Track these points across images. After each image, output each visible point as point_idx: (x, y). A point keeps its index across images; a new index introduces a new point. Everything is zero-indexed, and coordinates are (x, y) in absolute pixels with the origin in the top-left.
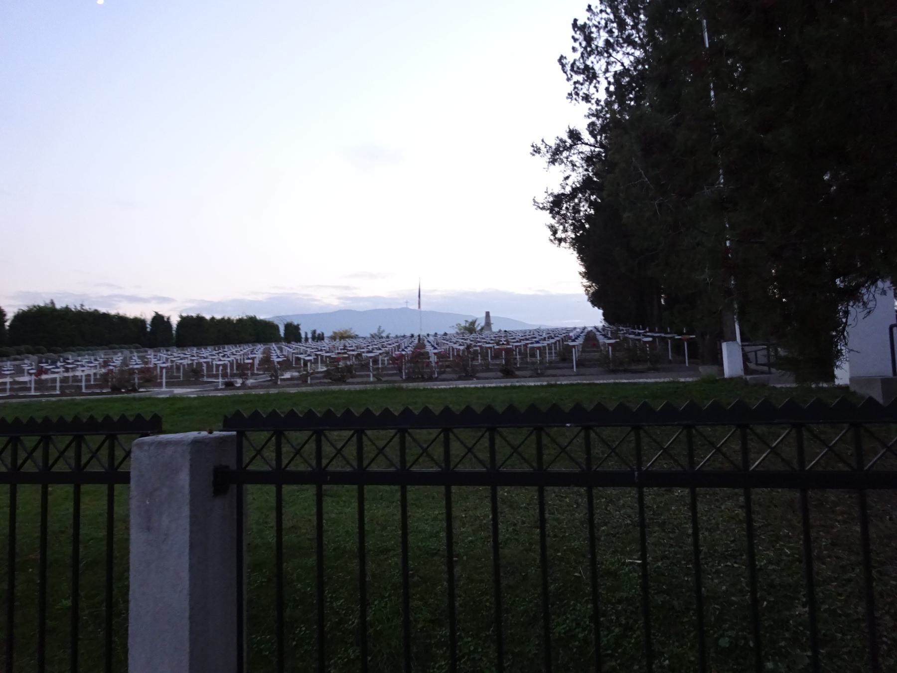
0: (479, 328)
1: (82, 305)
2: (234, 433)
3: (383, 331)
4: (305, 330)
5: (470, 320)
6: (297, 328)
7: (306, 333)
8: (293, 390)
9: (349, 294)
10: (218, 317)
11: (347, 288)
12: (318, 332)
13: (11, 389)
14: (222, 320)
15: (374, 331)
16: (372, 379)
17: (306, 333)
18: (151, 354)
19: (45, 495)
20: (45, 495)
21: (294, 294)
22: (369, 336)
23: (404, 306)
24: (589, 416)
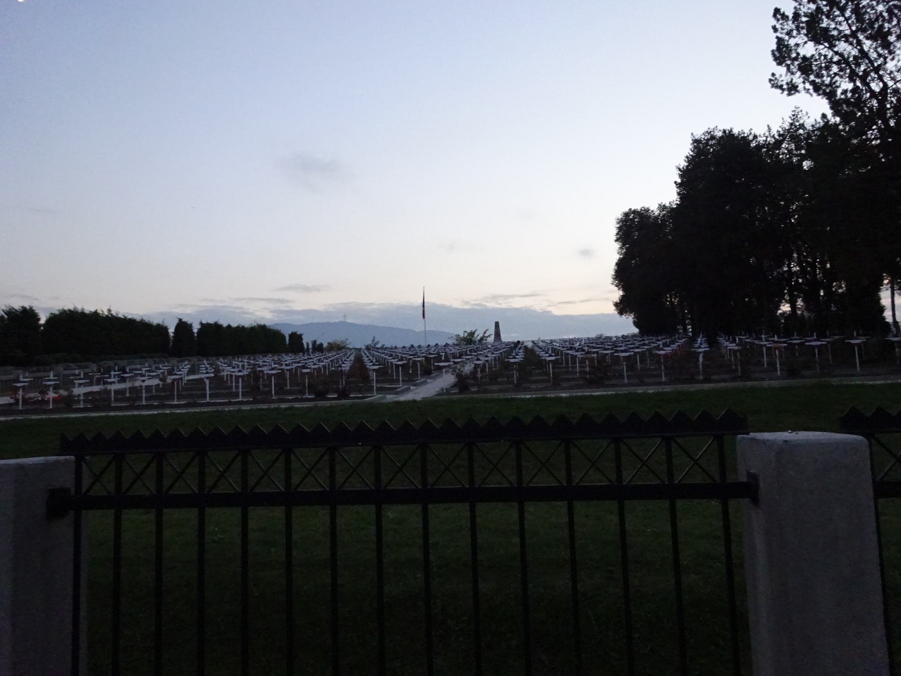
0: (479, 338)
1: (109, 310)
2: (73, 457)
3: (378, 343)
4: (307, 340)
5: (469, 331)
6: (299, 337)
7: (308, 344)
8: (246, 408)
9: (283, 307)
10: (234, 325)
11: (281, 301)
12: (318, 343)
13: (85, 401)
14: (238, 327)
15: (369, 342)
16: (664, 379)
17: (308, 344)
18: (221, 362)
19: (425, 511)
20: (425, 511)
21: (224, 307)
22: (364, 347)
23: (342, 319)
24: (619, 426)
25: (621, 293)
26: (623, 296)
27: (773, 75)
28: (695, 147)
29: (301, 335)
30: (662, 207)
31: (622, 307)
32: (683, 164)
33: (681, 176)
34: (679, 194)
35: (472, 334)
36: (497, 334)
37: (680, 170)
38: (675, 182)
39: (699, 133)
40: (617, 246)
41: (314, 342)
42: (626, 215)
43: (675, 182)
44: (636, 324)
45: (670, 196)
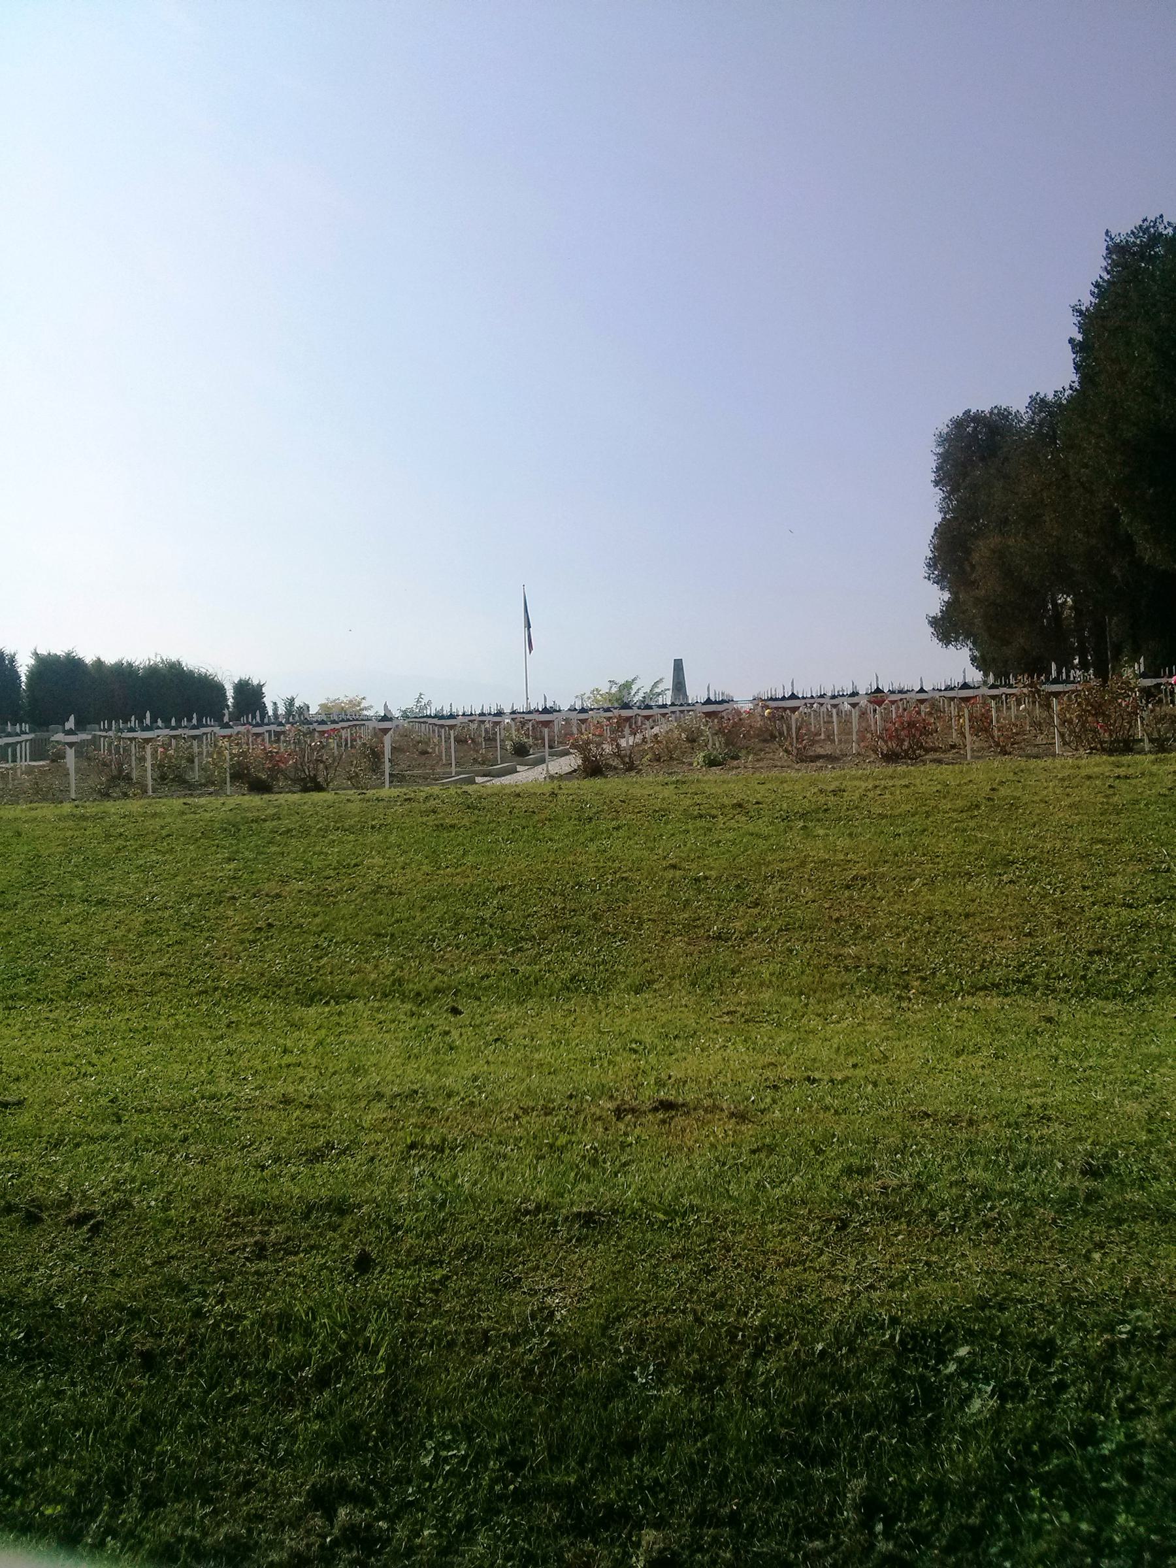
4: (274, 698)
25: (946, 596)
26: (948, 604)
27: (1161, 216)
28: (1115, 264)
29: (260, 686)
30: (1039, 404)
31: (947, 627)
32: (1087, 300)
33: (1083, 328)
34: (1077, 367)
35: (627, 686)
36: (679, 685)
37: (1080, 312)
38: (1071, 341)
39: (1124, 227)
40: (936, 495)
41: (291, 702)
42: (959, 424)
43: (1071, 341)
44: (980, 663)
45: (1057, 375)
